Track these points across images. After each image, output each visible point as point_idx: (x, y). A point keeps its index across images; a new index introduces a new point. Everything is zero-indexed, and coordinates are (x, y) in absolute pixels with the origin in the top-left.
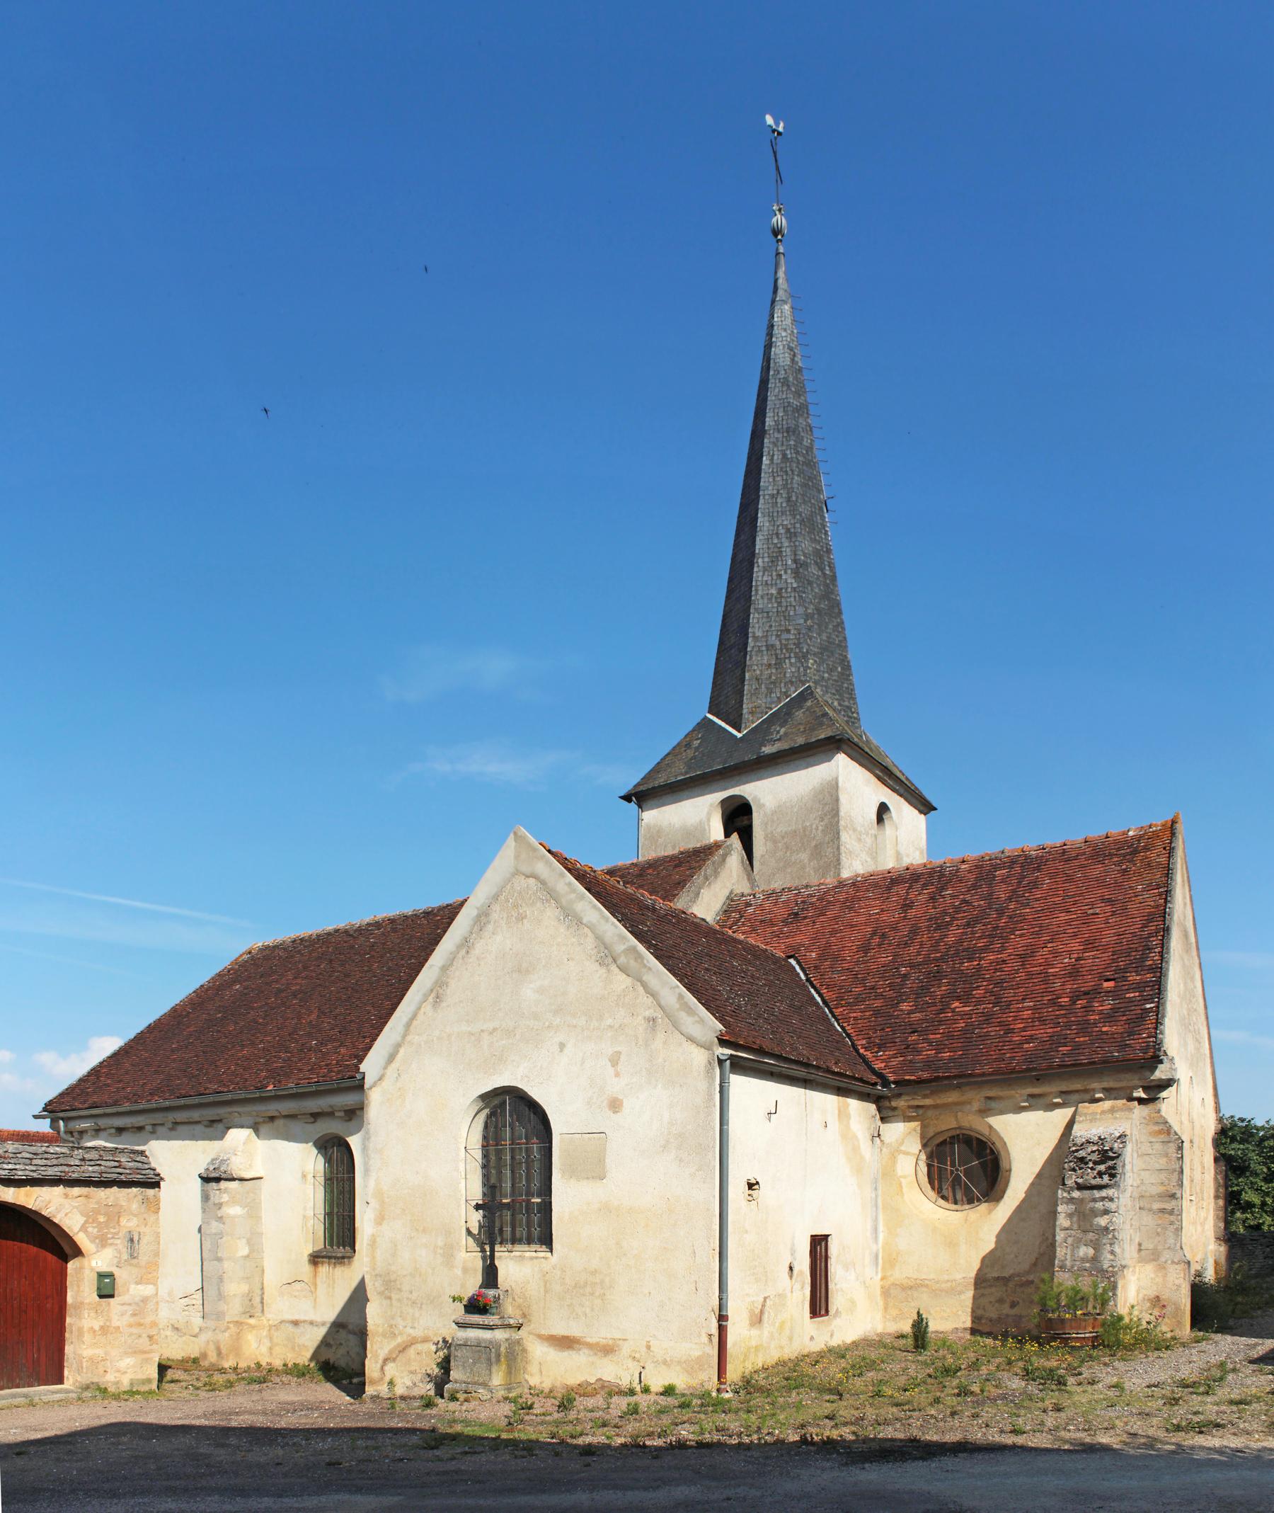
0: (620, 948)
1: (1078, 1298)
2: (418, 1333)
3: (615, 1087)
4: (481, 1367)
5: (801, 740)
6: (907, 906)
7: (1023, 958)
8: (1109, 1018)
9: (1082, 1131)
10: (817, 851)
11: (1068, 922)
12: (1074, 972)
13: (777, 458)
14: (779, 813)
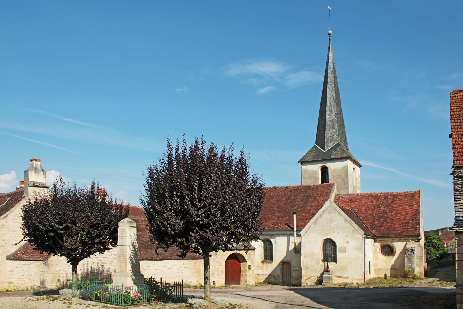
0: (348, 220)
1: (409, 271)
2: (312, 275)
3: (348, 240)
4: (328, 280)
5: (339, 156)
6: (372, 202)
7: (396, 215)
8: (412, 228)
9: (408, 246)
10: (343, 180)
11: (403, 209)
12: (405, 219)
13: (331, 89)
14: (335, 171)
